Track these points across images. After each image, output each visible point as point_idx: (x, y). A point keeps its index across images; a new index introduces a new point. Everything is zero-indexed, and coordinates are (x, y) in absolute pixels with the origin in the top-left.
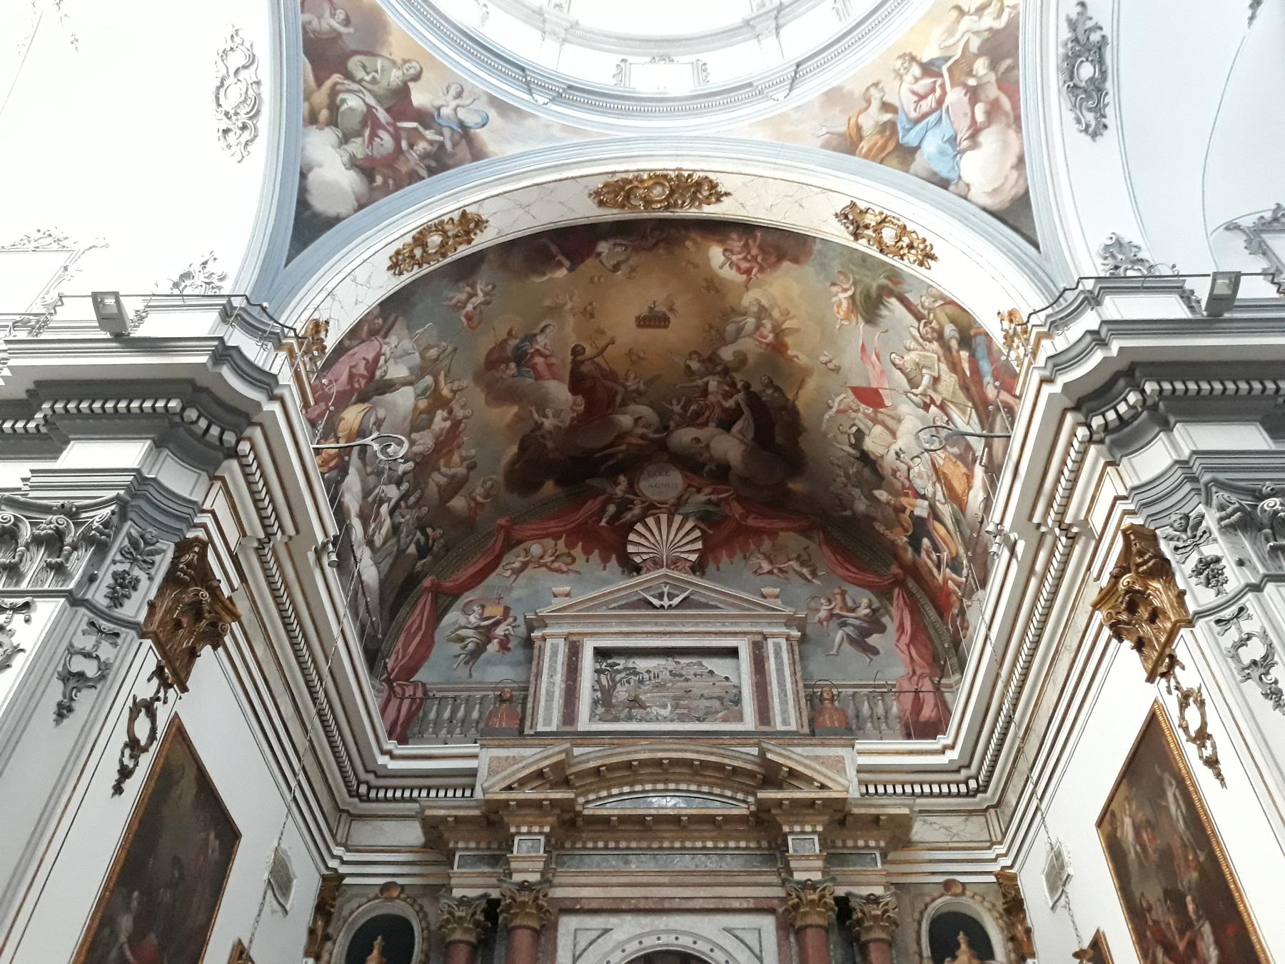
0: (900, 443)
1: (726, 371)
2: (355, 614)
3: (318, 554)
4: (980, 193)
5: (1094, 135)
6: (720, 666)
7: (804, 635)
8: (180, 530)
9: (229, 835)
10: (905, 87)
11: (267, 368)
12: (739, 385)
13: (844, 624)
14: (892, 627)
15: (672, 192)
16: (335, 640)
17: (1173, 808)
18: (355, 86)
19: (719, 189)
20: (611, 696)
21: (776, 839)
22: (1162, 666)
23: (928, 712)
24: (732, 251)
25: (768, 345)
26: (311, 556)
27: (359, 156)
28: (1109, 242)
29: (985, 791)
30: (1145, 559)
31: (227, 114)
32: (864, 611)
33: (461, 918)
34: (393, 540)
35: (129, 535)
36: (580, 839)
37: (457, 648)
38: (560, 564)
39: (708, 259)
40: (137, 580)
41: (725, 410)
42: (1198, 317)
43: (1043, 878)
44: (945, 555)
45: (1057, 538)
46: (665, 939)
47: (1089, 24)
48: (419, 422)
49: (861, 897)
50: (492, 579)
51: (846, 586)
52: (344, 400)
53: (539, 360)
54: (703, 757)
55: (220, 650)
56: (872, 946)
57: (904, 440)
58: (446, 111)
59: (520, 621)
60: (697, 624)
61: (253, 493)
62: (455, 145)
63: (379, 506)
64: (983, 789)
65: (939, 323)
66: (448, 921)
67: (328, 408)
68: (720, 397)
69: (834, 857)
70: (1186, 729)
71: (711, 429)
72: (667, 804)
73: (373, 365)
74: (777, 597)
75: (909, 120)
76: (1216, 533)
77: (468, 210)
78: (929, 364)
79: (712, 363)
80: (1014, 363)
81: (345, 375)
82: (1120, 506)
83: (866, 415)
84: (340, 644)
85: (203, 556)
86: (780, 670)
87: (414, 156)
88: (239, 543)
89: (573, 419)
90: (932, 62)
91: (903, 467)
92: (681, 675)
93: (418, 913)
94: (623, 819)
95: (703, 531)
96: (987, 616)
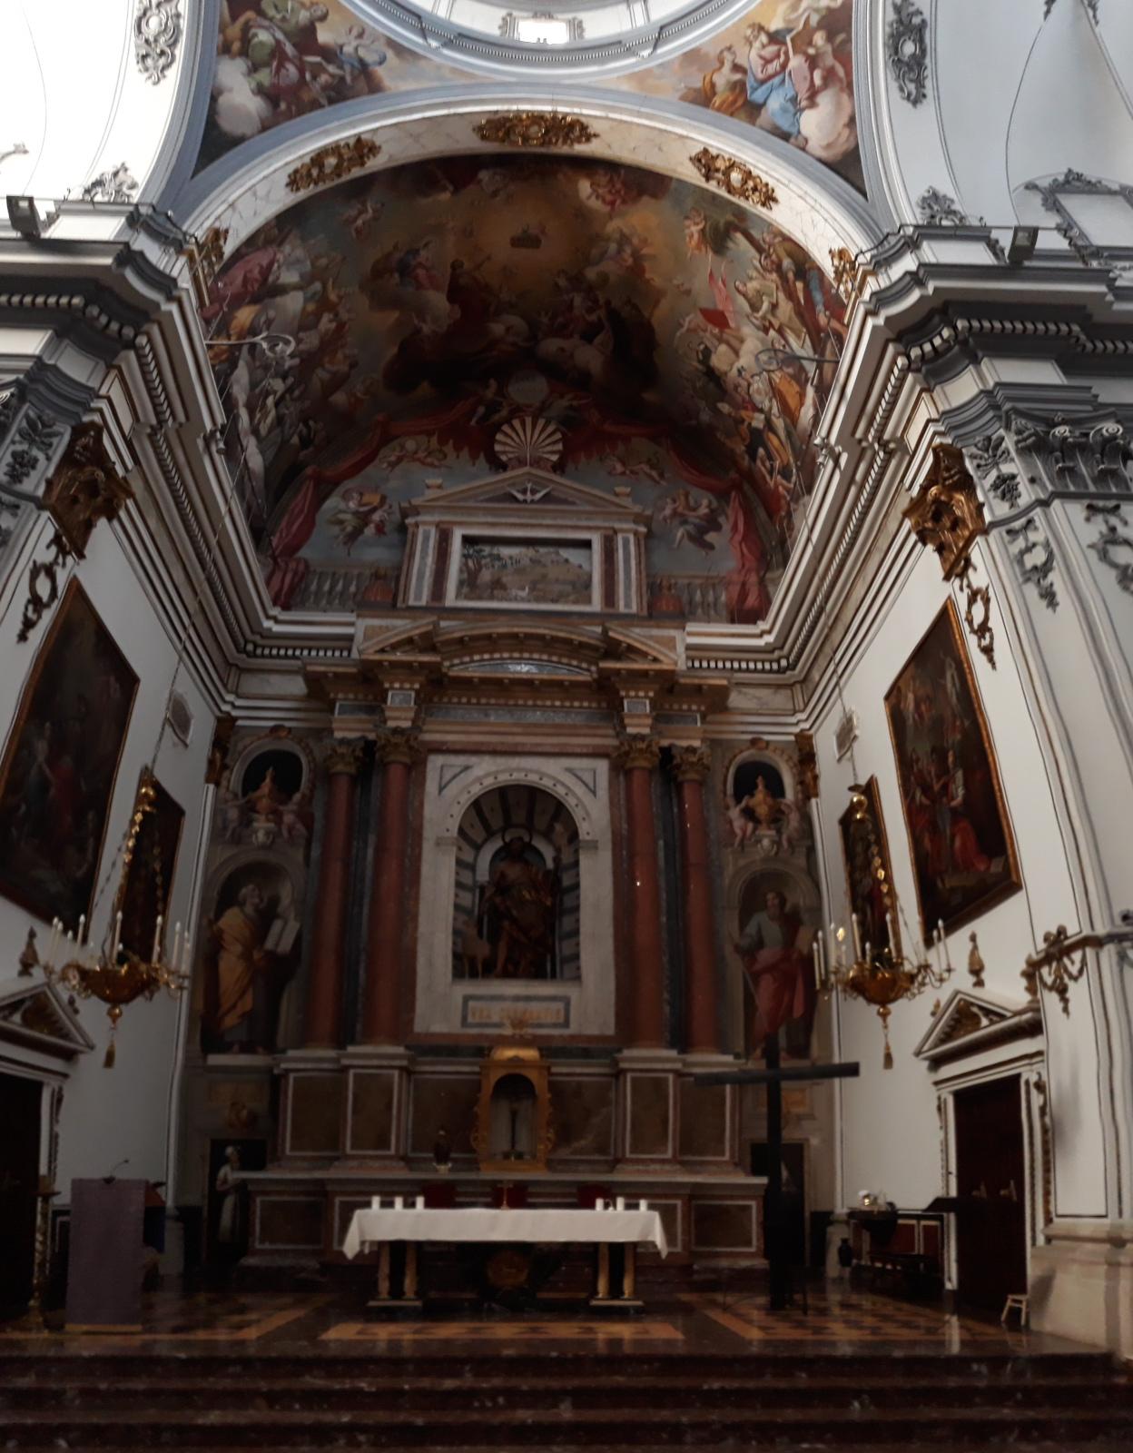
2: (242, 496)
3: (208, 440)
5: (915, 102)
6: (574, 556)
7: (650, 531)
8: (77, 414)
9: (128, 681)
10: (753, 54)
11: (167, 271)
12: (602, 302)
14: (727, 527)
15: (547, 131)
16: (222, 518)
17: (949, 685)
18: (266, 23)
20: (476, 578)
22: (957, 566)
23: (752, 600)
26: (200, 443)
28: (926, 195)
30: (950, 471)
31: (147, 41)
33: (343, 754)
34: (277, 431)
35: (27, 416)
37: (336, 530)
39: (577, 191)
40: (36, 460)
42: (1002, 264)
43: (834, 739)
44: (777, 464)
45: (875, 453)
46: (515, 776)
47: (911, 9)
48: (306, 323)
50: (370, 470)
52: (237, 302)
53: (421, 272)
54: (554, 633)
55: (115, 523)
56: (686, 785)
57: (745, 360)
58: (348, 49)
59: (396, 508)
62: (354, 79)
63: (266, 397)
64: (791, 667)
65: (778, 256)
66: (331, 756)
67: (221, 308)
69: (661, 717)
70: (970, 622)
72: (523, 669)
73: (266, 271)
74: (628, 495)
75: (756, 79)
76: (1013, 454)
77: (363, 137)
79: (577, 281)
81: (239, 277)
83: (714, 336)
84: (227, 521)
85: (99, 439)
86: (627, 561)
87: (316, 87)
88: (133, 428)
90: (777, 32)
91: (744, 384)
94: (484, 681)
95: (563, 434)
96: (813, 516)
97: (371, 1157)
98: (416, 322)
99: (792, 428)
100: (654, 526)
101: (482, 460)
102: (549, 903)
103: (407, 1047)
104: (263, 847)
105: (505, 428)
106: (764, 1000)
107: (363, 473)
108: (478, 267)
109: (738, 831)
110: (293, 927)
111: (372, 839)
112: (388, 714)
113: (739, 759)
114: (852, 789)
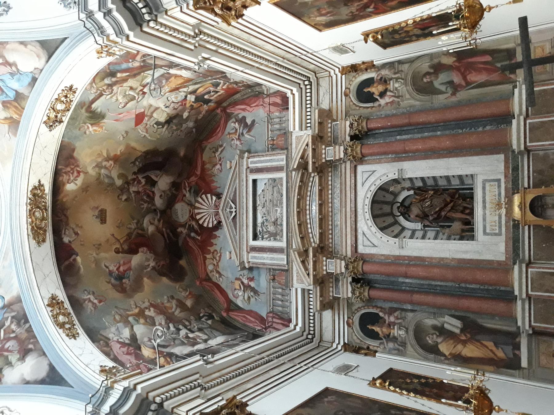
0: (162, 106)
1: (127, 183)
3: (208, 363)
4: (40, 63)
5: (9, 8)
6: (260, 187)
9: (326, 392)
11: (121, 392)
12: (134, 177)
13: (242, 134)
19: (37, 185)
20: (273, 233)
21: (328, 165)
23: (278, 100)
24: (69, 180)
25: (115, 163)
26: (209, 366)
27: (18, 356)
28: (63, 5)
29: (309, 78)
32: (237, 125)
33: (360, 293)
34: (205, 330)
36: (328, 245)
37: (252, 300)
38: (217, 256)
41: (146, 182)
44: (212, 89)
45: (201, 39)
46: (366, 210)
49: (350, 130)
50: (223, 286)
51: (226, 132)
52: (139, 357)
53: (121, 269)
54: (296, 194)
55: (248, 403)
57: (160, 104)
59: (242, 273)
60: (243, 197)
61: (180, 394)
62: (13, 311)
64: (308, 79)
65: (104, 86)
66: (361, 299)
68: (140, 186)
69: (335, 142)
71: (155, 190)
72: (315, 208)
73: (123, 344)
74: (231, 162)
77: (46, 303)
78: (124, 91)
79: (123, 189)
80: (122, 53)
82: (185, 9)
83: (148, 120)
87: (18, 330)
89: (150, 252)
91: (172, 105)
92: (264, 204)
93: (358, 311)
94: (321, 227)
96: (239, 73)
98: (149, 269)
99: (194, 82)
100: (245, 149)
101: (217, 233)
102: (432, 192)
103: (514, 264)
104: (407, 332)
106: (481, 78)
107: (225, 289)
108: (118, 240)
109: (391, 100)
110: (447, 319)
111: (401, 280)
114: (366, 42)
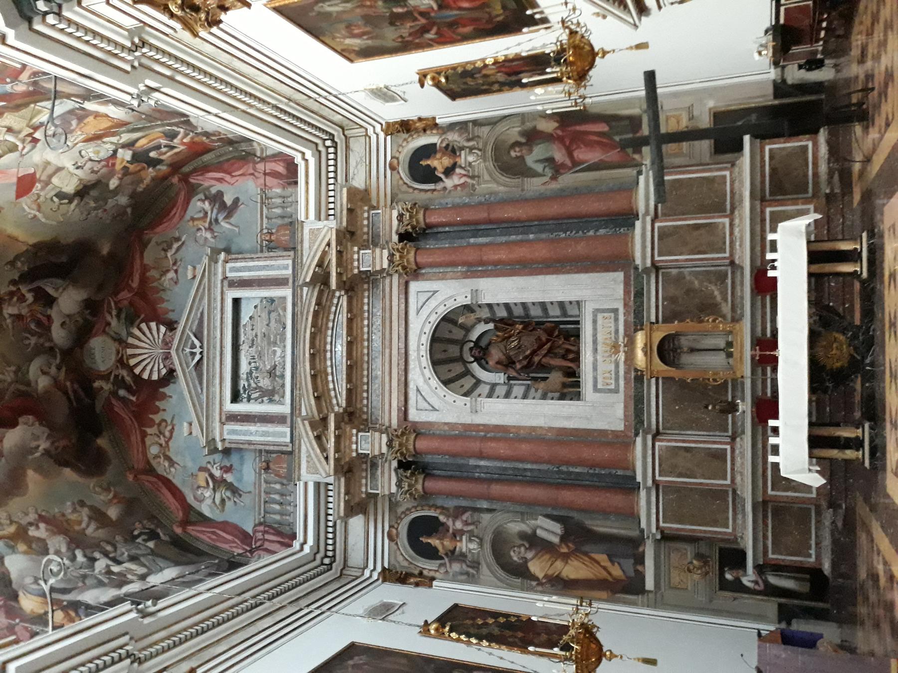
9: (352, 650)
23: (280, 168)
33: (409, 486)
37: (229, 504)
44: (163, 142)
46: (423, 353)
50: (177, 481)
54: (309, 325)
56: (428, 221)
57: (67, 161)
59: (210, 458)
63: (112, 573)
64: (332, 137)
66: (411, 494)
69: (374, 242)
72: (340, 349)
74: (194, 268)
83: (43, 189)
95: (141, 322)
96: (211, 119)
97: (733, 464)
98: (37, 454)
100: (221, 246)
102: (521, 327)
103: (637, 435)
104: (481, 544)
105: (137, 371)
109: (462, 180)
110: (542, 521)
111: (472, 462)
112: (377, 453)
113: (408, 181)
